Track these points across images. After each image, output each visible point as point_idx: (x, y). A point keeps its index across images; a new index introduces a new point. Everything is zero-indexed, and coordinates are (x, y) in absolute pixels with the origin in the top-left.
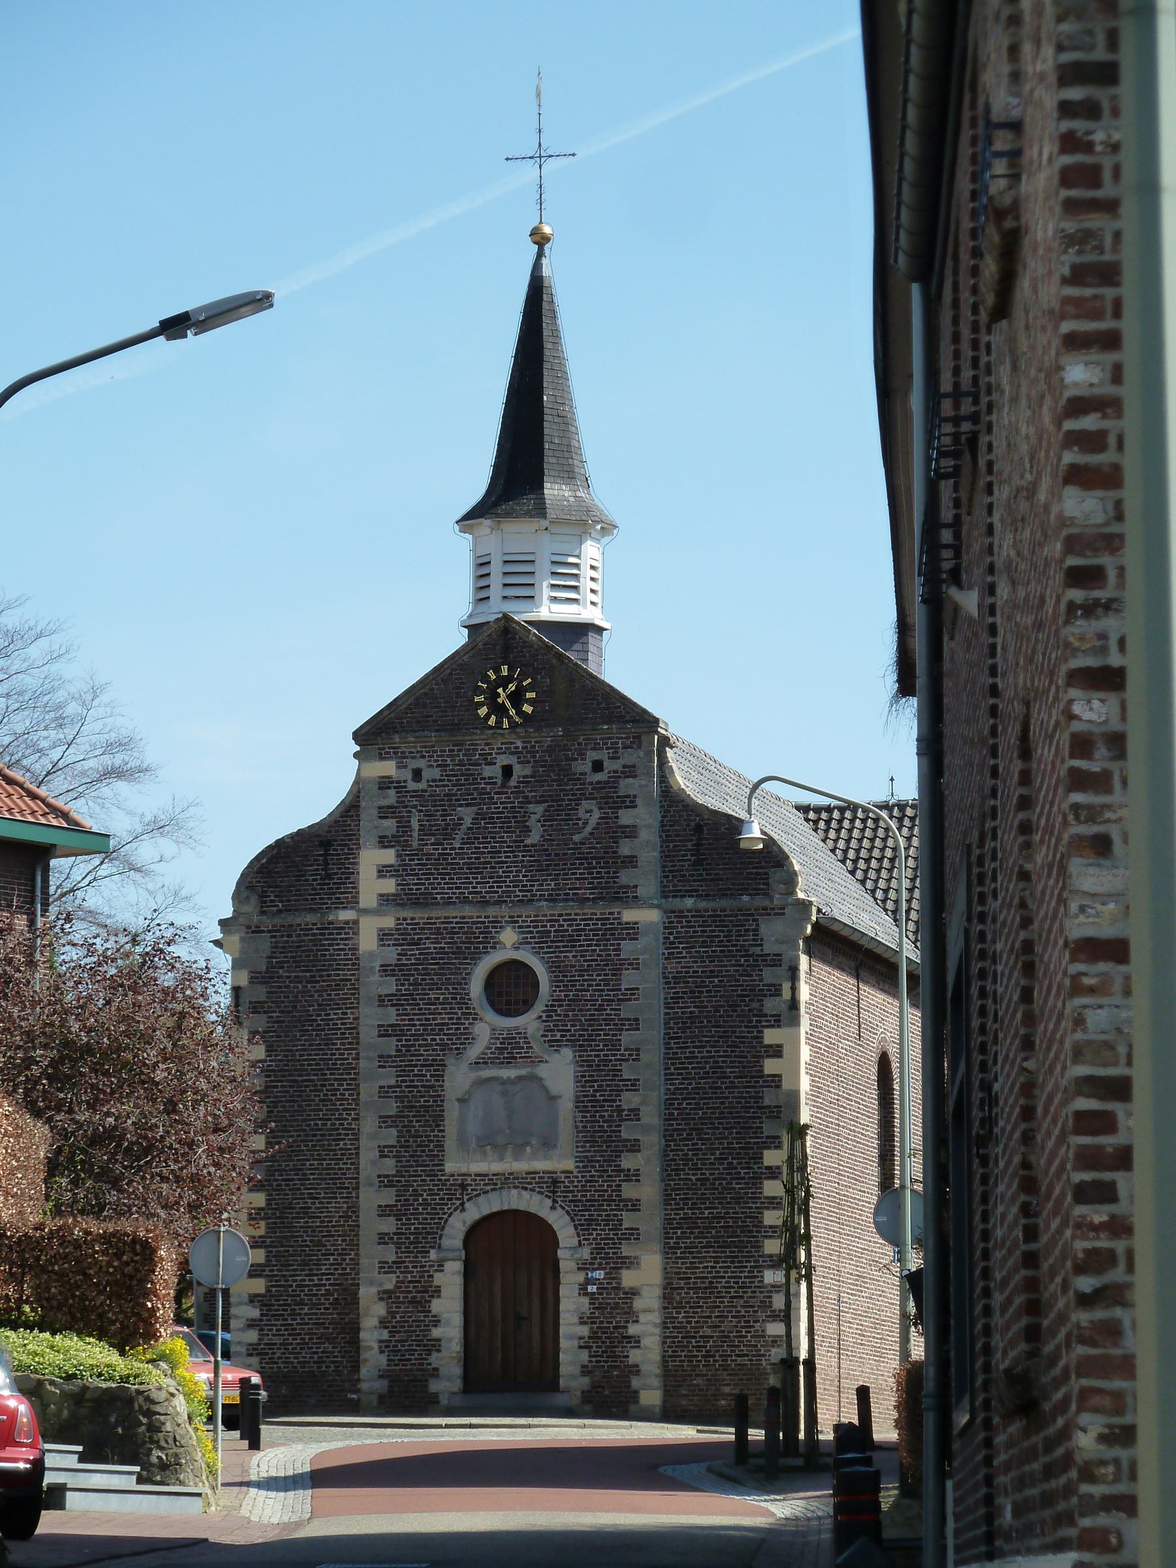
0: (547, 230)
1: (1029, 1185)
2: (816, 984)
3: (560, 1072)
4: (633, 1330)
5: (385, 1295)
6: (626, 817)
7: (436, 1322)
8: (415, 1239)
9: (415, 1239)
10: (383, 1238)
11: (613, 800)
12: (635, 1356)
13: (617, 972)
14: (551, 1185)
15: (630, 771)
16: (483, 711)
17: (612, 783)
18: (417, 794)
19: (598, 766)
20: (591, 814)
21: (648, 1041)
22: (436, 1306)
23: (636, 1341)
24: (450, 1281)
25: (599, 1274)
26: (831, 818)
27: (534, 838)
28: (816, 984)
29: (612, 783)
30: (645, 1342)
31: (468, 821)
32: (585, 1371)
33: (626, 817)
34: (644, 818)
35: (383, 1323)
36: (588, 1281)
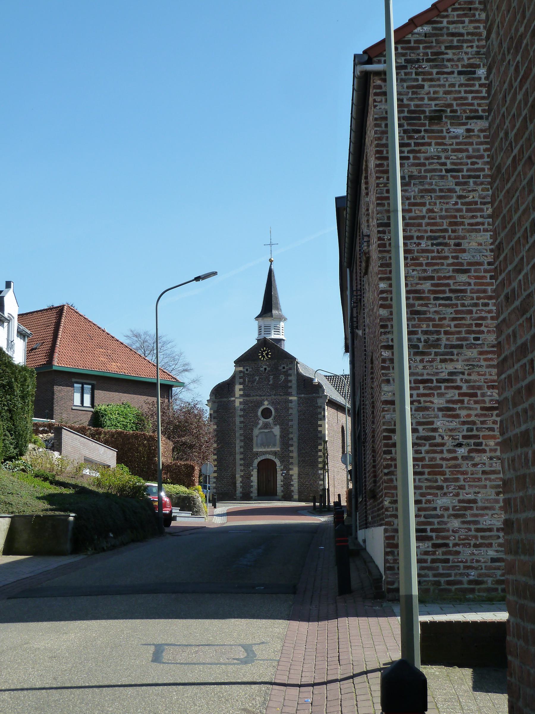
0: (272, 259)
1: (374, 451)
2: (329, 412)
3: (277, 431)
4: (292, 483)
5: (241, 476)
6: (290, 378)
7: (252, 482)
8: (247, 465)
9: (247, 465)
10: (241, 465)
11: (287, 375)
12: (292, 488)
13: (288, 410)
14: (275, 453)
15: (290, 369)
16: (260, 357)
17: (287, 371)
18: (247, 374)
19: (284, 368)
20: (282, 378)
21: (295, 424)
22: (252, 478)
23: (293, 485)
24: (255, 473)
25: (285, 472)
26: (332, 378)
27: (271, 383)
28: (329, 412)
29: (287, 371)
30: (294, 485)
31: (257, 379)
32: (282, 491)
33: (290, 378)
34: (293, 378)
35: (241, 482)
36: (283, 473)
